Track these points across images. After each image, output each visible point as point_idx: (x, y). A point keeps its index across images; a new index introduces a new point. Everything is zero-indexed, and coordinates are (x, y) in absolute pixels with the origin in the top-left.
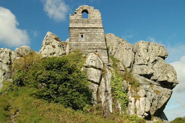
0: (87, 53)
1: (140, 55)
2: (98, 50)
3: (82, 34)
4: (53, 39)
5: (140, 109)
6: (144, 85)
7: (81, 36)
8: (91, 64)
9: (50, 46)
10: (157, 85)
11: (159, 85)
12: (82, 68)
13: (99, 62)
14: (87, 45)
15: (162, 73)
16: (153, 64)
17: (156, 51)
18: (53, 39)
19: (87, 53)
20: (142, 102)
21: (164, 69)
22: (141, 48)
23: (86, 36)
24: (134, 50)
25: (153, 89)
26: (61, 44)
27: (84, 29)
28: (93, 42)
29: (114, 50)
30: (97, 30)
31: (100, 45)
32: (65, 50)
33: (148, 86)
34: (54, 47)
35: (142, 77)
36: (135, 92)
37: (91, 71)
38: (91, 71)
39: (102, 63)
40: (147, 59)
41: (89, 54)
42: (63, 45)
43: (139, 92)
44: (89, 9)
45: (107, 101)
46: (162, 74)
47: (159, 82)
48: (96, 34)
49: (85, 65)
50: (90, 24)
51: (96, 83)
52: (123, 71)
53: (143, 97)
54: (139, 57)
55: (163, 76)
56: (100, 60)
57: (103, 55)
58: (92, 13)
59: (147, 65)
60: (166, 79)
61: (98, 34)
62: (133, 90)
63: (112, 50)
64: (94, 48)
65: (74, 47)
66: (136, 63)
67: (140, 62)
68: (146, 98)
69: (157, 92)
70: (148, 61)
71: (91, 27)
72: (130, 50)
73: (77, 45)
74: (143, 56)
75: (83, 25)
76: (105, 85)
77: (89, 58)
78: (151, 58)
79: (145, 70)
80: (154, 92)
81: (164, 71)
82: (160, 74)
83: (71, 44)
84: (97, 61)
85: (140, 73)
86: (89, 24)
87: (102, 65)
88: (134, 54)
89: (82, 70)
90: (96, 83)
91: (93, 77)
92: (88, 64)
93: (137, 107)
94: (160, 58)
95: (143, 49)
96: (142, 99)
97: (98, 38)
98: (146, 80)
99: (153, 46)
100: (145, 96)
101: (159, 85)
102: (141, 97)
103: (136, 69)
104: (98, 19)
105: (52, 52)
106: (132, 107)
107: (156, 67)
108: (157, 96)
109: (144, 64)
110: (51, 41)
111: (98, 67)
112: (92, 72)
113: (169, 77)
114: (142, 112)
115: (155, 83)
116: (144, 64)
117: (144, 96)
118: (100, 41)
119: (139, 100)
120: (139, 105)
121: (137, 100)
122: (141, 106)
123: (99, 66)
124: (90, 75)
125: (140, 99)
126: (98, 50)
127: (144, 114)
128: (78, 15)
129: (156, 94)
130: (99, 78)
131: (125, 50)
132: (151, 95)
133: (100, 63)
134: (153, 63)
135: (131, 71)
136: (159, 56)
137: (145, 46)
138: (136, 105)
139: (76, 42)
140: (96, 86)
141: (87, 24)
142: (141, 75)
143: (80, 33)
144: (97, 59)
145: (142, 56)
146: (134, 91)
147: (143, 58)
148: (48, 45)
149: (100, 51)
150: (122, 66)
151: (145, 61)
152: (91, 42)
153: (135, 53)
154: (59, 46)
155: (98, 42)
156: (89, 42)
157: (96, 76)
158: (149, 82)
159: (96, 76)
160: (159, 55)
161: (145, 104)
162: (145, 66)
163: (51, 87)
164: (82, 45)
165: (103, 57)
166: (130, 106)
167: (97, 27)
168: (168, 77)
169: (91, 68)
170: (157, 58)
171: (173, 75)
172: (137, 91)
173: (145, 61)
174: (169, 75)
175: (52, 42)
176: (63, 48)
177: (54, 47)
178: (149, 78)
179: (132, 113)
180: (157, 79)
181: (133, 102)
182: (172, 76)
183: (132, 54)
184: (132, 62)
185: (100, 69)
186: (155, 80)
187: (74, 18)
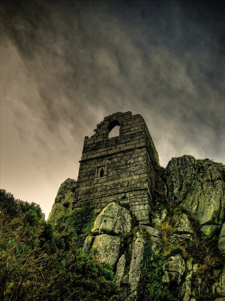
2: (128, 195)
3: (102, 169)
31: (133, 182)
43: (216, 284)
50: (121, 146)
57: (137, 203)
61: (132, 162)
71: (122, 149)
104: (137, 131)
126: (128, 195)
141: (113, 147)
149: (131, 195)
159: (106, 251)
165: (138, 206)
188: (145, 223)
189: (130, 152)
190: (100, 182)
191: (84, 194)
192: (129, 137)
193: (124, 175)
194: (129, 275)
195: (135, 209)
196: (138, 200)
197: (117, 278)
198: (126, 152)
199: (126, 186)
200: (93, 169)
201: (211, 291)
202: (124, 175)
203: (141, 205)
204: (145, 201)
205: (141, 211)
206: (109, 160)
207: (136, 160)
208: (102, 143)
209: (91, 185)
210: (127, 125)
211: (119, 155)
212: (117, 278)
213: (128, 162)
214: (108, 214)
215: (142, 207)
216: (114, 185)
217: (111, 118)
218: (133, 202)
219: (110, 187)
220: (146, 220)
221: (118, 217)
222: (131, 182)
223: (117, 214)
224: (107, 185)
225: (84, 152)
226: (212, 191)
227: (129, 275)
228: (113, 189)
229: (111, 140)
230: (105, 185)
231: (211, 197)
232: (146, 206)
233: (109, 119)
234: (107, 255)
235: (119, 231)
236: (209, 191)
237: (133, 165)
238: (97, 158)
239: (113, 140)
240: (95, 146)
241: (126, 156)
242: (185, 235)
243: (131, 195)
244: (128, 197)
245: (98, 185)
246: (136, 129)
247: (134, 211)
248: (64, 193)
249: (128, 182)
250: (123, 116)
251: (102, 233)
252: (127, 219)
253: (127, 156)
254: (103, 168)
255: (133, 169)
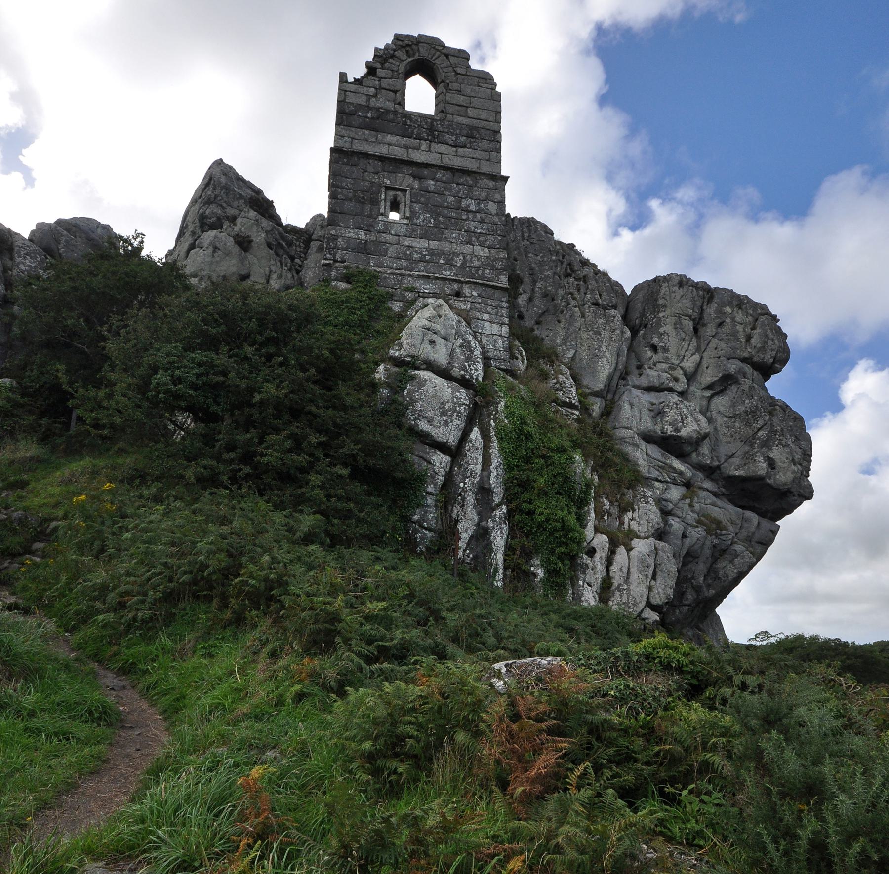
0: (409, 295)
1: (655, 340)
2: (466, 290)
3: (395, 197)
4: (241, 202)
5: (628, 590)
6: (657, 484)
7: (388, 204)
8: (425, 351)
9: (224, 237)
10: (715, 494)
11: (723, 494)
12: (381, 368)
13: (465, 345)
14: (416, 256)
15: (750, 441)
16: (708, 394)
17: (735, 334)
18: (241, 202)
19: (409, 295)
20: (642, 561)
21: (761, 423)
22: (668, 312)
23: (417, 207)
24: (635, 316)
25: (697, 506)
26: (283, 238)
27: (405, 169)
28: (447, 247)
29: (537, 301)
30: (470, 186)
31: (477, 263)
32: (298, 272)
33: (675, 493)
34: (244, 243)
35: (654, 451)
36: (615, 511)
37: (422, 384)
38: (422, 384)
39: (477, 353)
40: (689, 364)
41: (420, 302)
42: (290, 244)
43: (630, 514)
44: (446, 63)
45: (482, 535)
46: (747, 448)
47: (724, 478)
48: (464, 204)
49: (394, 353)
50: (443, 148)
51: (442, 447)
52: (571, 406)
53: (647, 538)
54: (649, 353)
55: (748, 457)
56: (471, 338)
57: (486, 316)
58: (455, 86)
59: (682, 394)
60: (761, 467)
61: (473, 207)
62: (605, 501)
63: (530, 300)
64: (447, 274)
65: (349, 255)
66: (634, 379)
67: (652, 375)
68: (660, 544)
69: (713, 526)
70: (691, 377)
71: (447, 161)
72: (613, 312)
73: (363, 249)
74: (673, 350)
75: (406, 147)
76: (480, 461)
77: (420, 319)
78: (705, 363)
79: (672, 415)
80: (699, 522)
81: (760, 433)
82: (737, 447)
83: (335, 238)
84: (460, 341)
85: (647, 424)
86: (435, 147)
87: (480, 366)
88: (628, 333)
89: (377, 376)
90: (442, 447)
91: (430, 414)
92: (413, 351)
93: (617, 580)
94: (748, 369)
95: (679, 316)
96: (641, 547)
97: (472, 225)
98: (669, 462)
99: (728, 310)
100: (661, 535)
101: (723, 494)
102: (638, 537)
103: (632, 405)
104: (483, 124)
105: (234, 269)
106: (590, 576)
107: (722, 409)
108: (708, 543)
109: (671, 390)
110: (231, 212)
111: (456, 372)
112: (428, 387)
113: (779, 464)
114: (635, 604)
115: (708, 484)
116: (671, 390)
117: (653, 536)
118: (482, 245)
119: (629, 549)
120: (625, 570)
121: (622, 550)
122: (635, 576)
123: (464, 369)
124: (418, 406)
125: (635, 542)
126: (466, 290)
127: (644, 615)
128: (385, 83)
129: (704, 534)
130: (458, 423)
131: (589, 312)
132: (684, 536)
133: (472, 352)
134: (709, 387)
135: (607, 412)
136: (744, 360)
137: (688, 304)
138: (614, 568)
139: (362, 233)
140: (440, 460)
141: (424, 145)
142: (648, 438)
143: (388, 188)
144: (458, 334)
145: (665, 350)
146: (612, 504)
147: (666, 360)
148: (212, 233)
149: (475, 293)
150: (569, 382)
151: (679, 373)
152: (434, 244)
153: (634, 332)
154: (269, 246)
155: (468, 249)
156: (424, 243)
157: (443, 414)
158: (681, 473)
159: (443, 414)
160: (746, 355)
161: (651, 569)
162: (675, 398)
163: (222, 438)
164: (392, 251)
165: (487, 324)
166: (584, 573)
167: (471, 165)
168: (771, 463)
169: (425, 374)
170: (733, 367)
171: (797, 457)
172: (625, 508)
173: (679, 373)
174: (776, 453)
175: (233, 220)
176: (292, 258)
177: (244, 243)
178: (682, 456)
179: (590, 598)
180: (718, 467)
181: (601, 555)
182: (793, 460)
183: (622, 332)
184: (618, 373)
185: (464, 383)
186: (710, 472)
187: (362, 100)
188: (502, 367)
189: (468, 178)
190: (393, 233)
191: (353, 250)
192: (465, 132)
193: (454, 235)
194: (491, 472)
195: (482, 328)
196: (489, 309)
197: (469, 475)
198: (457, 174)
199: (459, 265)
200: (372, 186)
201: (622, 523)
202: (454, 235)
203: (494, 323)
204: (502, 316)
205: (495, 337)
206: (415, 177)
207: (482, 206)
208: (391, 116)
209: (370, 231)
210: (459, 92)
211: (439, 175)
212: (469, 475)
213: (463, 204)
214: (438, 327)
215: (496, 328)
216: (432, 252)
217: (415, 47)
218: (479, 312)
219: (421, 253)
220: (504, 360)
221: (455, 339)
222: (471, 261)
223: (454, 331)
224: (412, 247)
225: (338, 124)
226: (604, 329)
227: (491, 472)
228: (428, 261)
229: (417, 120)
230: (406, 243)
231: (602, 342)
232: (504, 328)
233: (408, 45)
234: (446, 423)
235: (462, 372)
236: (598, 327)
237: (475, 216)
238: (381, 159)
239: (421, 122)
240: (372, 118)
241: (458, 184)
242: (570, 410)
243: (475, 293)
244: (469, 295)
245: (389, 238)
246: (482, 117)
247: (480, 333)
248: (224, 205)
249: (464, 257)
250: (447, 56)
251: (424, 366)
252: (474, 349)
253: (461, 187)
254: (399, 193)
255: (476, 228)
